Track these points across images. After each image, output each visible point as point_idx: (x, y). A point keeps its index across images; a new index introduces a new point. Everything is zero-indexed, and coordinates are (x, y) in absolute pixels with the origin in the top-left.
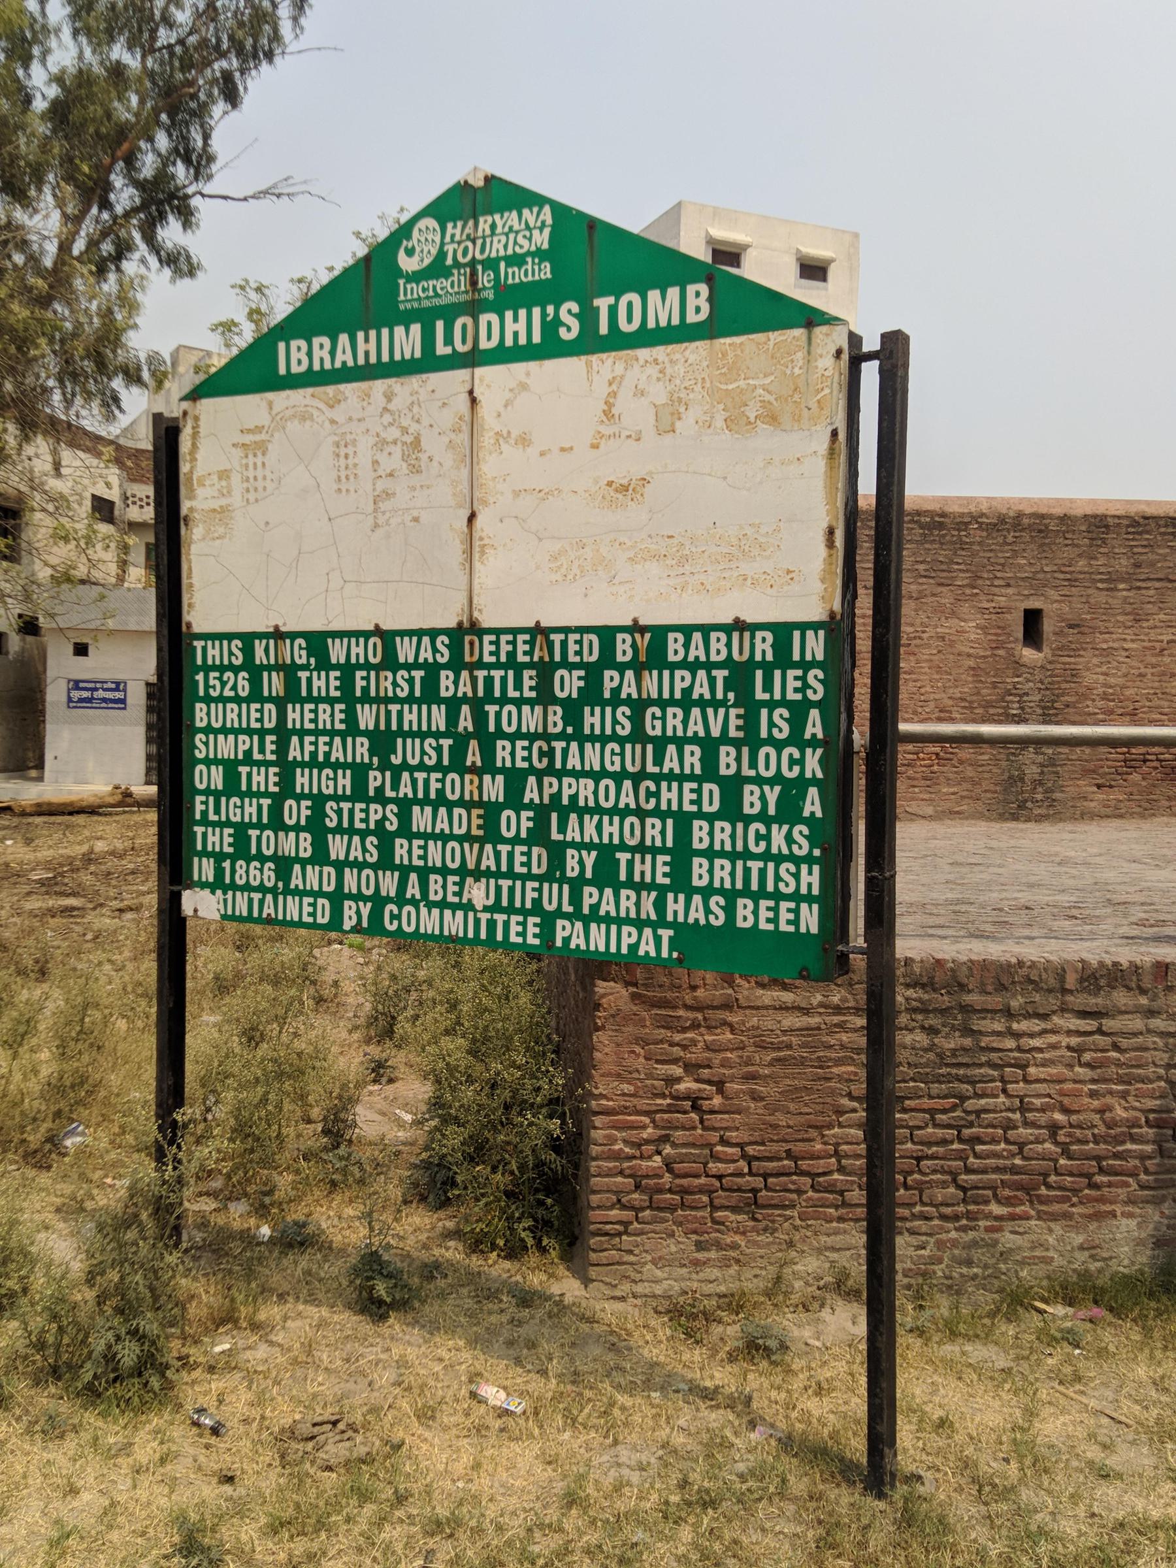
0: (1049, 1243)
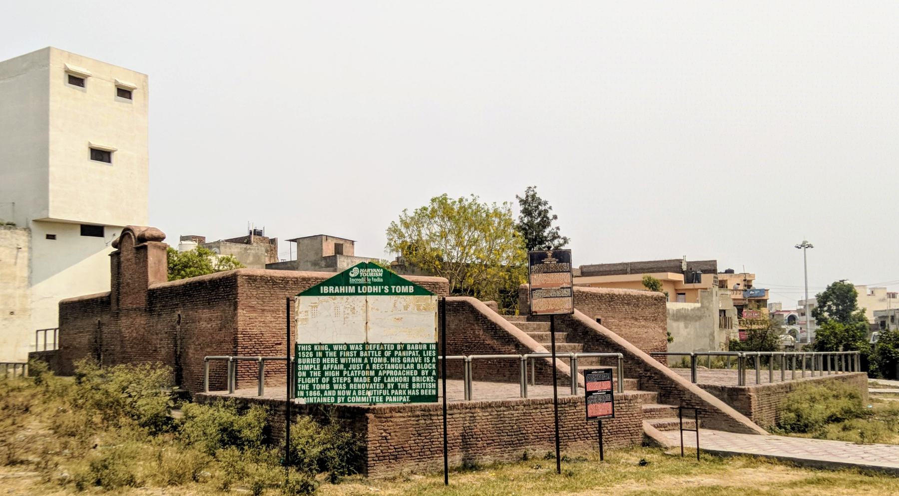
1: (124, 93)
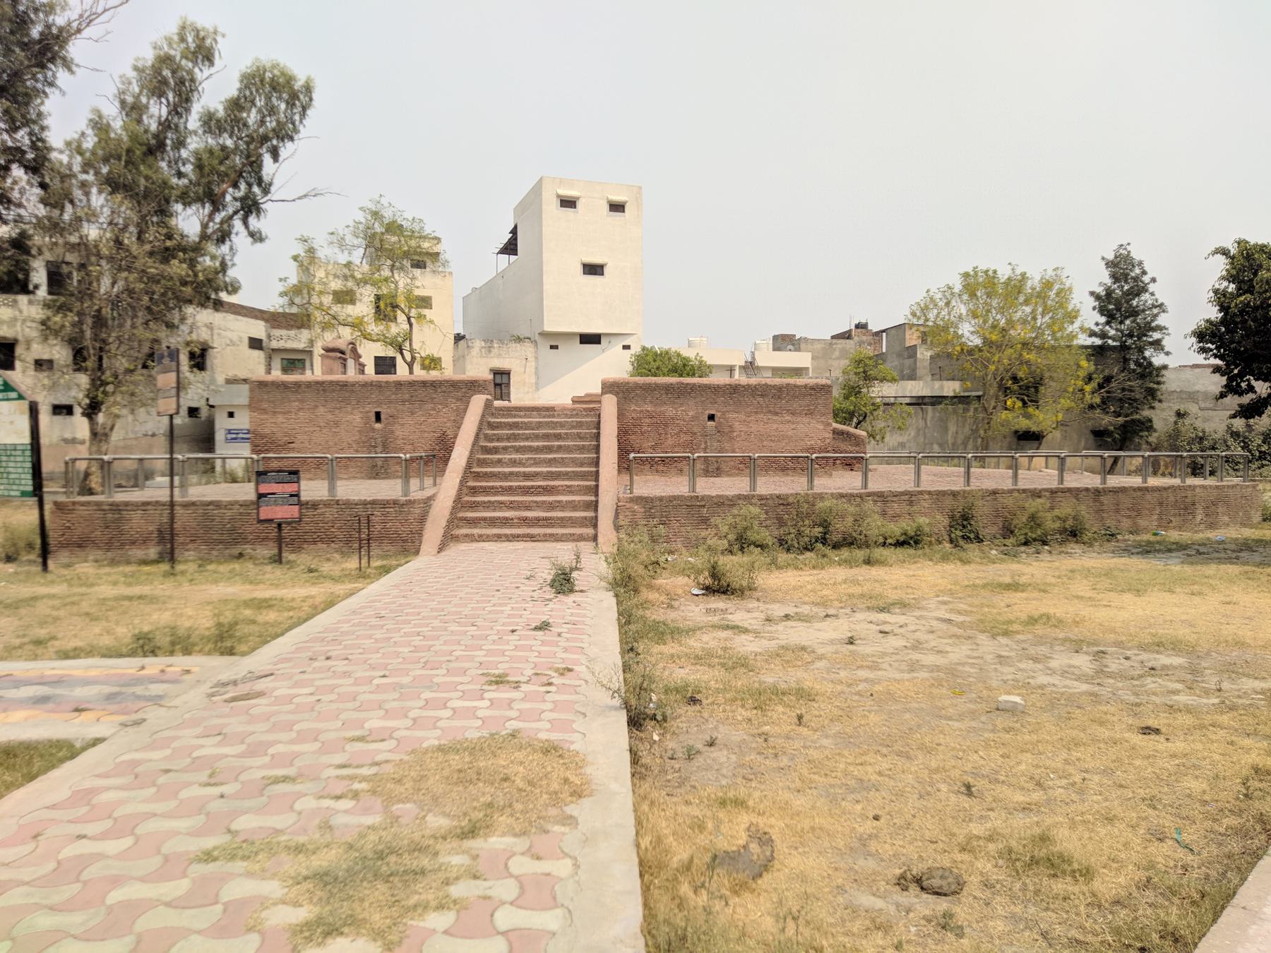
0: (138, 553)
1: (617, 207)
